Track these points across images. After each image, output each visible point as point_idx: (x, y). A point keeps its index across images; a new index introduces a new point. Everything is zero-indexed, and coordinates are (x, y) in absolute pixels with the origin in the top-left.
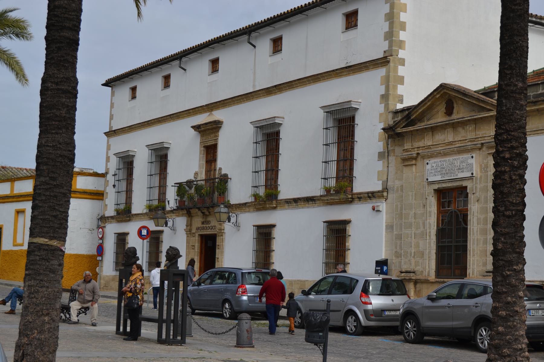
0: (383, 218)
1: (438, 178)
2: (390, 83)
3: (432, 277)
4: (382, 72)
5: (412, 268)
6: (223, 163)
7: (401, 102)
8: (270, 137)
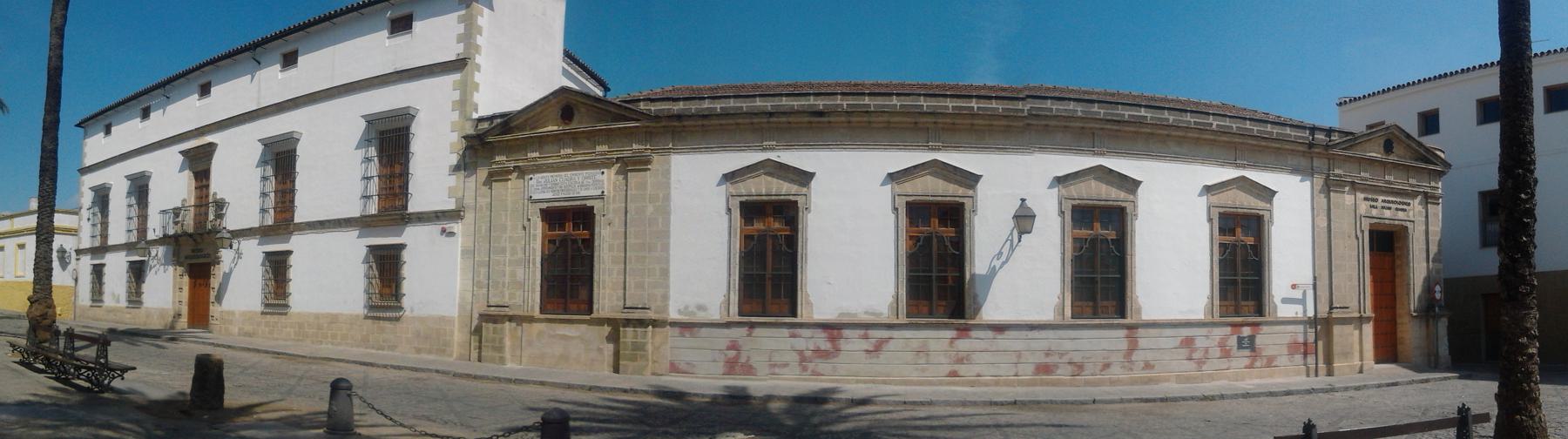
0: (458, 242)
1: (549, 195)
2: (466, 92)
3: (537, 313)
4: (457, 77)
5: (506, 301)
6: (219, 185)
7: (476, 110)
8: (281, 160)
